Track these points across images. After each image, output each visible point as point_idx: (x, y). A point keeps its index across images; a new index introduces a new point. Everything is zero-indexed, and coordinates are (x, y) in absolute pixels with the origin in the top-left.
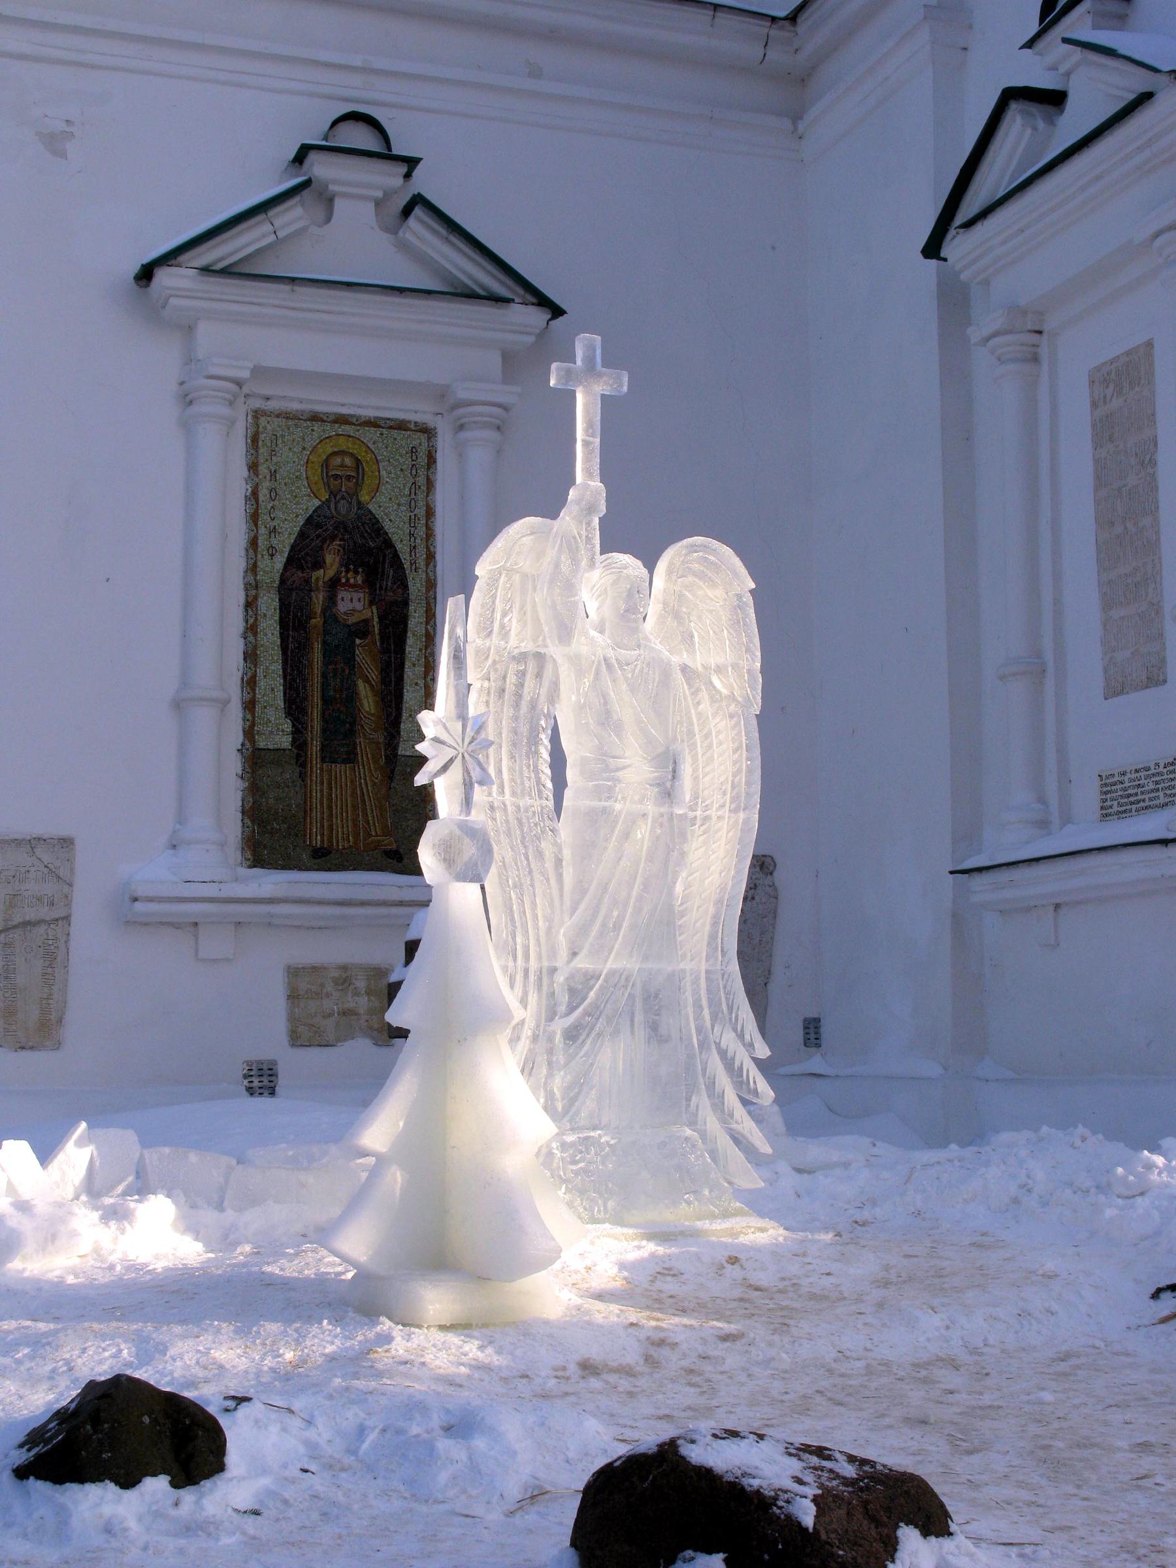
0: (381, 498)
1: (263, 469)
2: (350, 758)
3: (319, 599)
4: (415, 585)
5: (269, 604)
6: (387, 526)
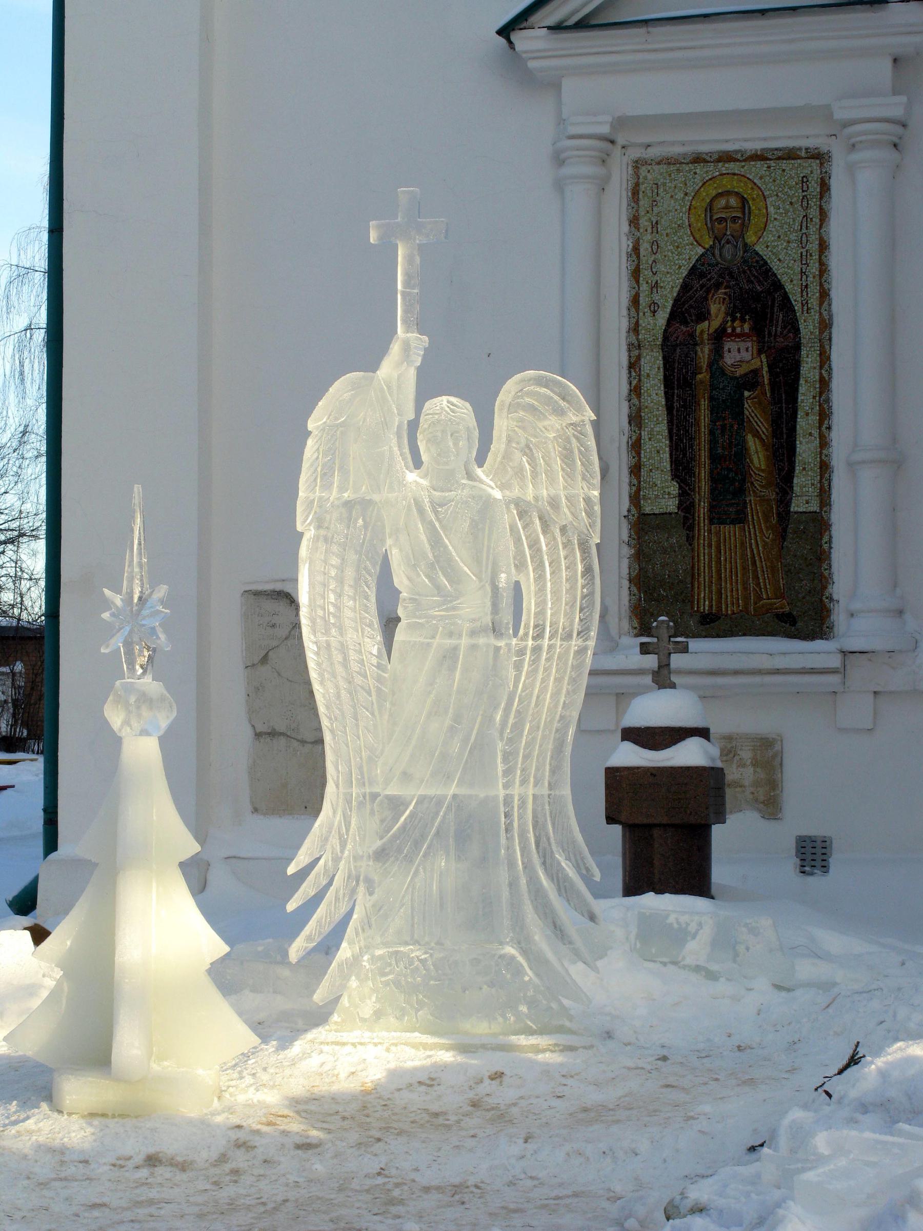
0: (769, 237)
1: (644, 222)
2: (740, 518)
3: (704, 353)
4: (808, 327)
5: (653, 363)
6: (775, 266)
